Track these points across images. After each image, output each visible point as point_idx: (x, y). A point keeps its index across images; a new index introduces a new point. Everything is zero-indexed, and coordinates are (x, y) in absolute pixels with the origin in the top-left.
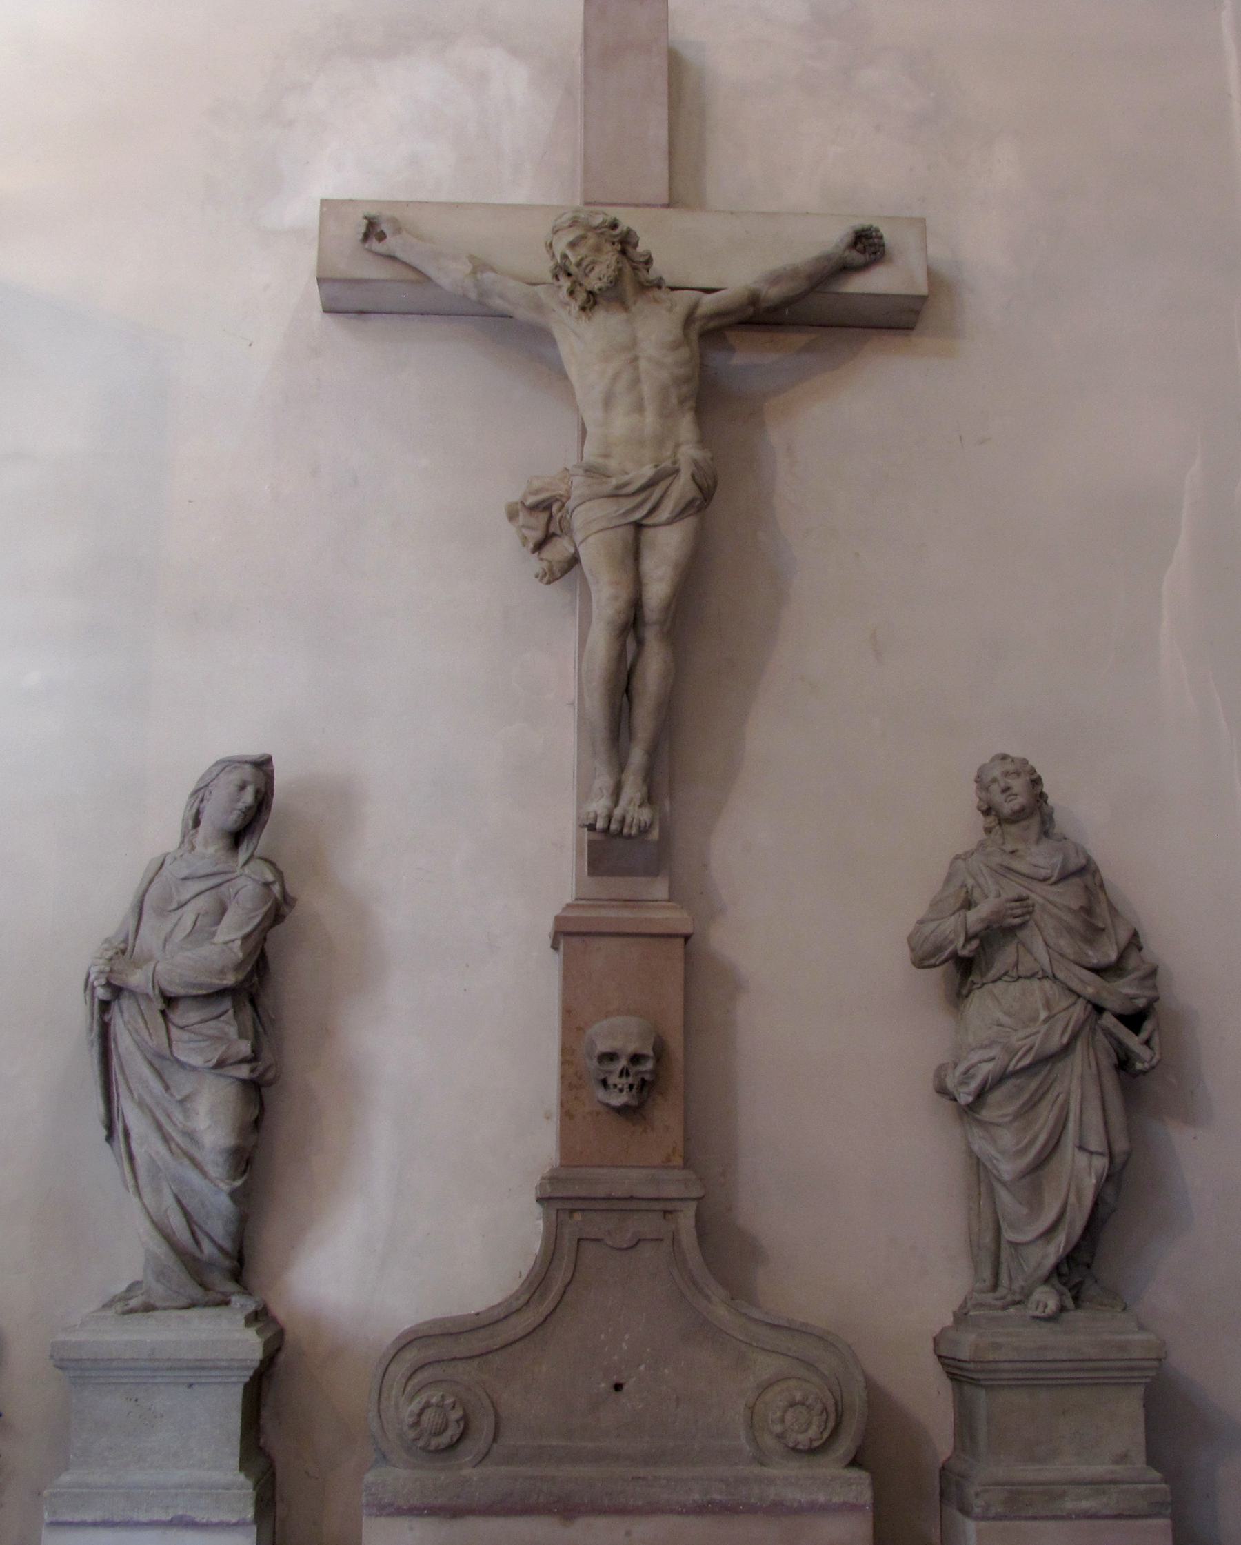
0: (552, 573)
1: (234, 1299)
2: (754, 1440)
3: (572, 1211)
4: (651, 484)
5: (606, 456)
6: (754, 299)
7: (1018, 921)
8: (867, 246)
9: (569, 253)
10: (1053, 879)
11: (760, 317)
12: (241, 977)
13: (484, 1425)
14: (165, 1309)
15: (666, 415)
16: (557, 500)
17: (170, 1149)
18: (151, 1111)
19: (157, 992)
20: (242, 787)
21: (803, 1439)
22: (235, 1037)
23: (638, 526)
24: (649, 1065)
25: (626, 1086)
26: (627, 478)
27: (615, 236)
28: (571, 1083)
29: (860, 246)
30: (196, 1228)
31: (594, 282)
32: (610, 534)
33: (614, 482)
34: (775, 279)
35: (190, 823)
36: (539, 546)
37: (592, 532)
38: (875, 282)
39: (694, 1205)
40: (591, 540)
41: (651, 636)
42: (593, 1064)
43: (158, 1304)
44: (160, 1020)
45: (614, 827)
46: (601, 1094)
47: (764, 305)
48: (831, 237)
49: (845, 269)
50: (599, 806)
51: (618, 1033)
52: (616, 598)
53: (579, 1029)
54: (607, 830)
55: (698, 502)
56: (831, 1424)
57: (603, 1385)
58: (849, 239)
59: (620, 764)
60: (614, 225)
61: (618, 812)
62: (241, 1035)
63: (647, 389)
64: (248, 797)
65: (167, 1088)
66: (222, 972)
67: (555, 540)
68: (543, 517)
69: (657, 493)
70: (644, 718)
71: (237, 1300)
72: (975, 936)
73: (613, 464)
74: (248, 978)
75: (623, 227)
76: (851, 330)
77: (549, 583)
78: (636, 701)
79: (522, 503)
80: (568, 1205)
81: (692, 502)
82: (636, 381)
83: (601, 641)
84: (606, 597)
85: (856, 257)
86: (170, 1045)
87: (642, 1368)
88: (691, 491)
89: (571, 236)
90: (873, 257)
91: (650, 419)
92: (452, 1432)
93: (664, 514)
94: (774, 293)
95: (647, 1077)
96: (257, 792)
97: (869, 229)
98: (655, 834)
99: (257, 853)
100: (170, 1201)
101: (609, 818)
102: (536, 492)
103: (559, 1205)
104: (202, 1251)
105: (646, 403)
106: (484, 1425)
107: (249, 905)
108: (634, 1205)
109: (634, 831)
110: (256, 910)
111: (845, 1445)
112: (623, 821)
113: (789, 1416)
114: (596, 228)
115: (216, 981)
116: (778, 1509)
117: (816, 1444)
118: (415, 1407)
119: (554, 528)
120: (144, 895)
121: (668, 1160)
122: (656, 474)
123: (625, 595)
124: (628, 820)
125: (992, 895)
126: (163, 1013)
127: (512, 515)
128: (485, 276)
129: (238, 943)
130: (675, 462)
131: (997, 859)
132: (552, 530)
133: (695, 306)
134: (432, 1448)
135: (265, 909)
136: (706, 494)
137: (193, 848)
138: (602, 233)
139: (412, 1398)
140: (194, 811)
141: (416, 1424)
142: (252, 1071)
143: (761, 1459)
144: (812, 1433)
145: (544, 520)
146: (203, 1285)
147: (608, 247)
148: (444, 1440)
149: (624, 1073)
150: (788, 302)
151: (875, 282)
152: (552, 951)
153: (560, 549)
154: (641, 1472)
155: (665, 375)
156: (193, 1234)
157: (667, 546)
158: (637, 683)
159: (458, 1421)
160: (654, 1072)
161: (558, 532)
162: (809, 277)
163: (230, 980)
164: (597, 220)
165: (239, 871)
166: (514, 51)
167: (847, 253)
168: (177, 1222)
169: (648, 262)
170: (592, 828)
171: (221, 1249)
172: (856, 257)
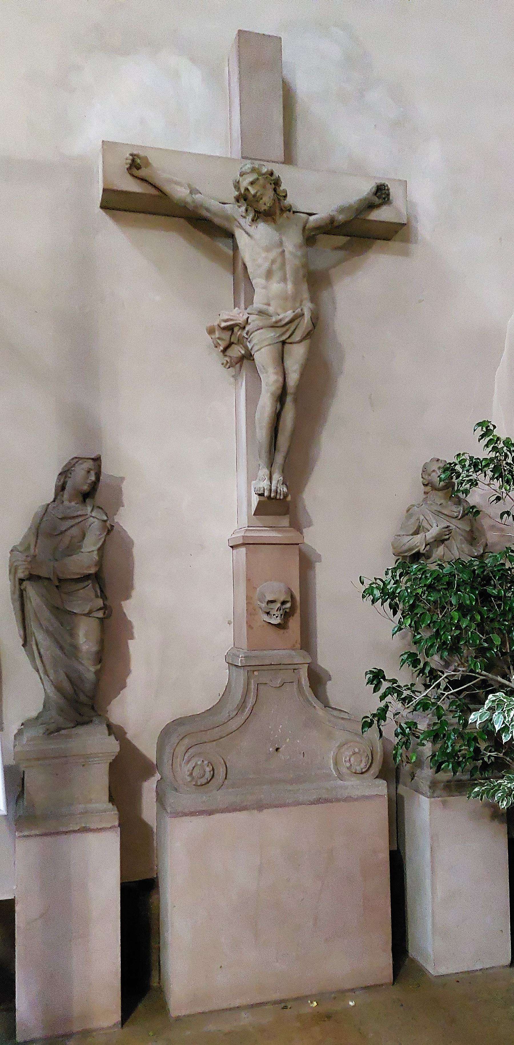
2: (337, 770)
3: (254, 671)
5: (269, 305)
6: (332, 220)
7: (447, 537)
8: (382, 194)
9: (250, 188)
10: (459, 517)
11: (331, 228)
12: (97, 569)
13: (221, 771)
21: (359, 769)
24: (288, 605)
25: (279, 615)
26: (280, 317)
28: (251, 612)
29: (379, 194)
31: (263, 208)
33: (274, 319)
34: (342, 210)
35: (60, 488)
37: (262, 346)
38: (382, 214)
39: (307, 665)
40: (263, 350)
42: (264, 605)
45: (272, 495)
46: (266, 618)
47: (336, 224)
48: (365, 188)
49: (371, 206)
50: (265, 484)
51: (274, 590)
52: (277, 381)
53: (254, 587)
54: (269, 497)
56: (370, 761)
57: (271, 749)
58: (374, 190)
59: (271, 464)
60: (272, 174)
62: (97, 596)
63: (289, 269)
66: (89, 567)
67: (233, 345)
72: (429, 544)
73: (271, 309)
75: (276, 174)
79: (218, 325)
80: (252, 668)
82: (283, 264)
84: (269, 380)
85: (377, 201)
87: (288, 740)
89: (250, 178)
92: (208, 776)
93: (297, 337)
94: (341, 218)
95: (288, 610)
97: (384, 185)
98: (289, 498)
102: (226, 321)
103: (249, 668)
106: (221, 771)
107: (98, 533)
108: (282, 667)
109: (282, 497)
110: (100, 535)
111: (375, 769)
112: (276, 492)
113: (352, 759)
116: (348, 799)
117: (364, 770)
118: (190, 766)
121: (294, 646)
123: (281, 379)
124: (279, 491)
125: (435, 525)
128: (197, 196)
129: (96, 552)
130: (302, 310)
131: (435, 508)
132: (232, 340)
133: (307, 222)
134: (199, 784)
139: (189, 761)
141: (191, 774)
143: (341, 776)
144: (363, 766)
147: (268, 186)
148: (204, 781)
149: (279, 609)
151: (382, 214)
153: (237, 351)
154: (290, 787)
157: (297, 354)
159: (210, 772)
160: (290, 608)
162: (357, 210)
163: (92, 571)
164: (264, 170)
168: (66, 685)
170: (261, 495)
172: (377, 201)
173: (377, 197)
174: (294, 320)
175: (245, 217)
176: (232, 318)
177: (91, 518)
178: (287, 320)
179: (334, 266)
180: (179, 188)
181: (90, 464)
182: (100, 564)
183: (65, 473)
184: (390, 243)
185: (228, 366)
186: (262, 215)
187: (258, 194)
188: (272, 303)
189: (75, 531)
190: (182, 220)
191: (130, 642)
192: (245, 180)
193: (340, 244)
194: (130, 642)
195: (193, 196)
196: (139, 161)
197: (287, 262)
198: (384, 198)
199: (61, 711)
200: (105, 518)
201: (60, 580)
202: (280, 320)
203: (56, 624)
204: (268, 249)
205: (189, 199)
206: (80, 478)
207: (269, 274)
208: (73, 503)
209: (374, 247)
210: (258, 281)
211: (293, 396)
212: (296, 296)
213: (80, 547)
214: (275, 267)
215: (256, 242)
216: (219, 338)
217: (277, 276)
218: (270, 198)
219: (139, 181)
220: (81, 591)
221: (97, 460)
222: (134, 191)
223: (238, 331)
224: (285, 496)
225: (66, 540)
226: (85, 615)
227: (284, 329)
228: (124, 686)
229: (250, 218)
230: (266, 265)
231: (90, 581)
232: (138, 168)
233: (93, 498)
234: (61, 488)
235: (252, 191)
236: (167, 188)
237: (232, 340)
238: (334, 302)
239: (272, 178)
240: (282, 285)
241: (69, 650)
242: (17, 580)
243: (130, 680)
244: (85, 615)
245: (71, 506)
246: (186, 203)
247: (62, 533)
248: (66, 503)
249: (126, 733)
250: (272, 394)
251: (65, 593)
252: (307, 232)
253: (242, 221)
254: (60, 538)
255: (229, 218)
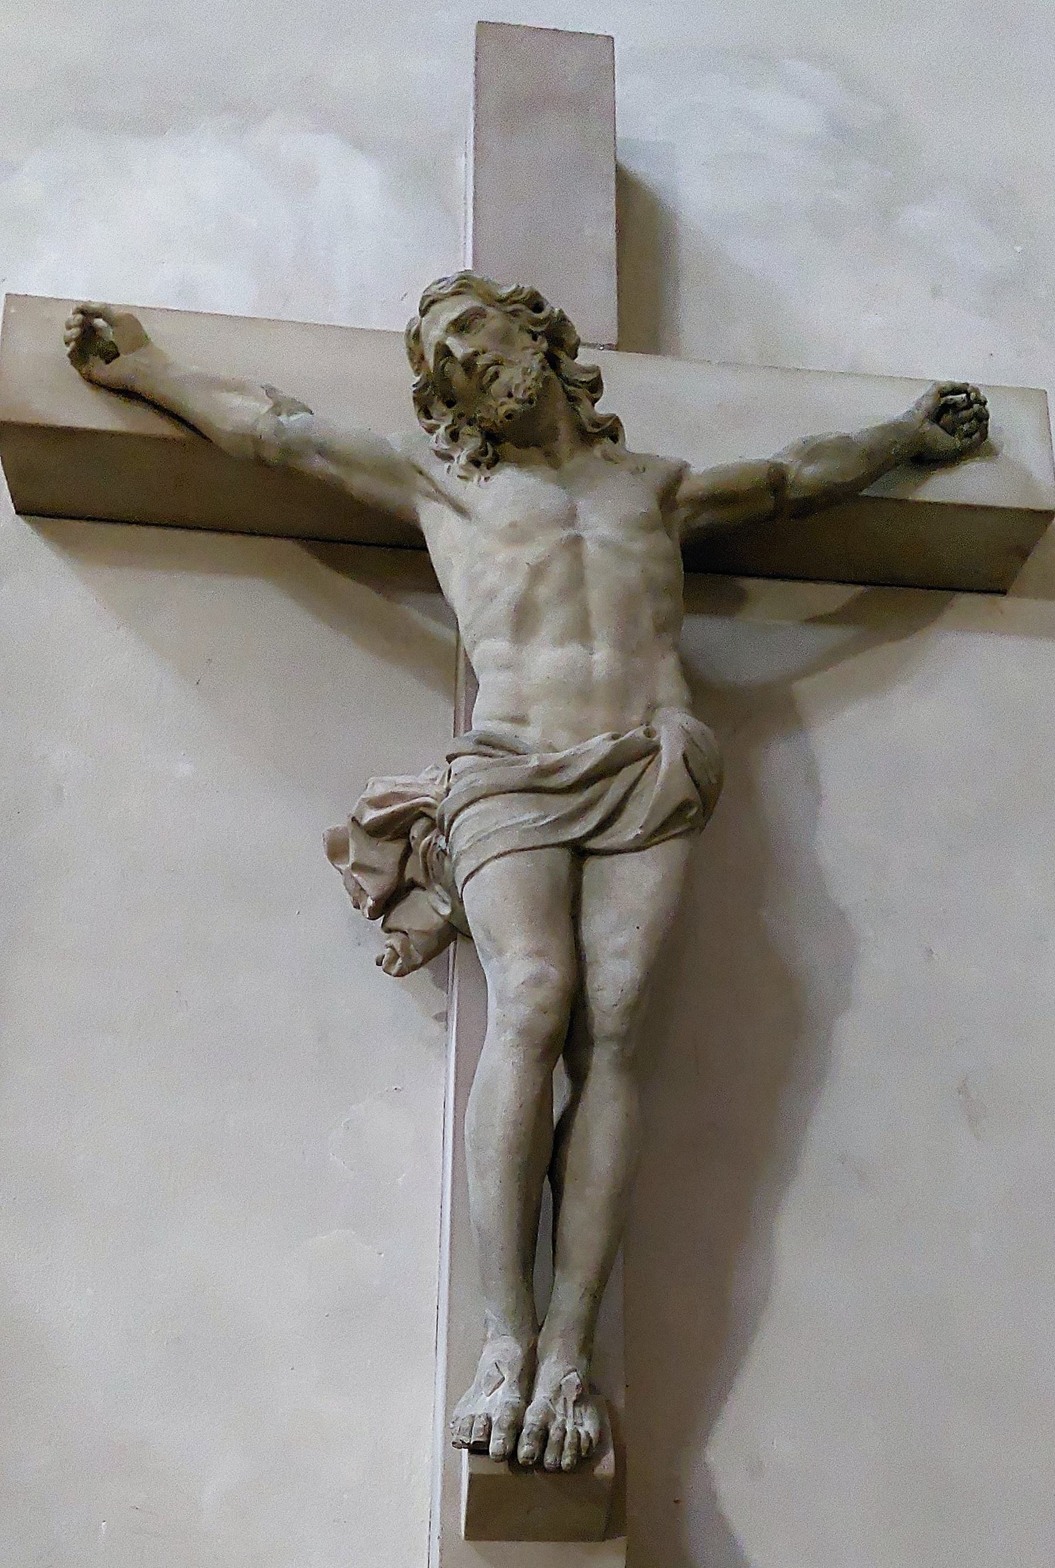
0: (408, 956)
4: (606, 770)
5: (520, 720)
8: (958, 421)
15: (627, 646)
16: (423, 815)
23: (579, 852)
27: (537, 323)
29: (947, 418)
31: (500, 406)
32: (522, 859)
33: (534, 761)
34: (812, 451)
36: (385, 906)
38: (964, 485)
41: (602, 1061)
47: (793, 495)
49: (925, 459)
50: (494, 1402)
52: (537, 981)
54: (510, 1457)
55: (692, 813)
59: (531, 1320)
61: (532, 1418)
63: (597, 597)
67: (415, 893)
68: (396, 849)
69: (616, 787)
70: (584, 1220)
73: (530, 735)
76: (912, 590)
77: (400, 974)
78: (569, 1188)
81: (683, 808)
83: (502, 1067)
84: (514, 973)
88: (682, 790)
89: (450, 311)
90: (967, 441)
91: (602, 657)
93: (628, 829)
101: (516, 1428)
102: (378, 803)
105: (595, 623)
109: (566, 1461)
114: (501, 301)
119: (414, 870)
122: (616, 749)
123: (556, 973)
124: (554, 1433)
127: (336, 851)
130: (649, 734)
132: (408, 875)
136: (702, 810)
138: (514, 313)
145: (399, 857)
150: (831, 499)
151: (964, 485)
152: (410, 408)
153: (425, 911)
155: (632, 573)
157: (629, 896)
158: (573, 1156)
161: (421, 879)
162: (870, 455)
166: (359, 144)
167: (927, 427)
169: (595, 387)
170: (478, 1449)
172: (942, 439)
173: (942, 427)
174: (619, 769)
175: (447, 457)
176: (401, 789)
178: (585, 765)
179: (807, 671)
180: (236, 400)
184: (1005, 603)
185: (394, 971)
186: (503, 441)
187: (481, 362)
188: (535, 712)
190: (288, 546)
192: (434, 321)
193: (833, 607)
195: (283, 418)
196: (110, 335)
197: (590, 576)
198: (969, 435)
202: (559, 767)
204: (517, 535)
205: (265, 428)
207: (523, 620)
209: (949, 615)
210: (487, 651)
211: (615, 1047)
212: (623, 690)
214: (544, 591)
215: (481, 531)
216: (356, 867)
217: (554, 620)
218: (525, 372)
219: (113, 399)
222: (93, 426)
223: (426, 833)
224: (587, 1456)
227: (577, 800)
229: (462, 457)
230: (512, 588)
232: (110, 355)
235: (459, 349)
236: (197, 404)
237: (408, 875)
238: (812, 780)
239: (541, 316)
240: (573, 650)
246: (257, 441)
250: (524, 1032)
252: (683, 513)
253: (439, 471)
255: (399, 471)
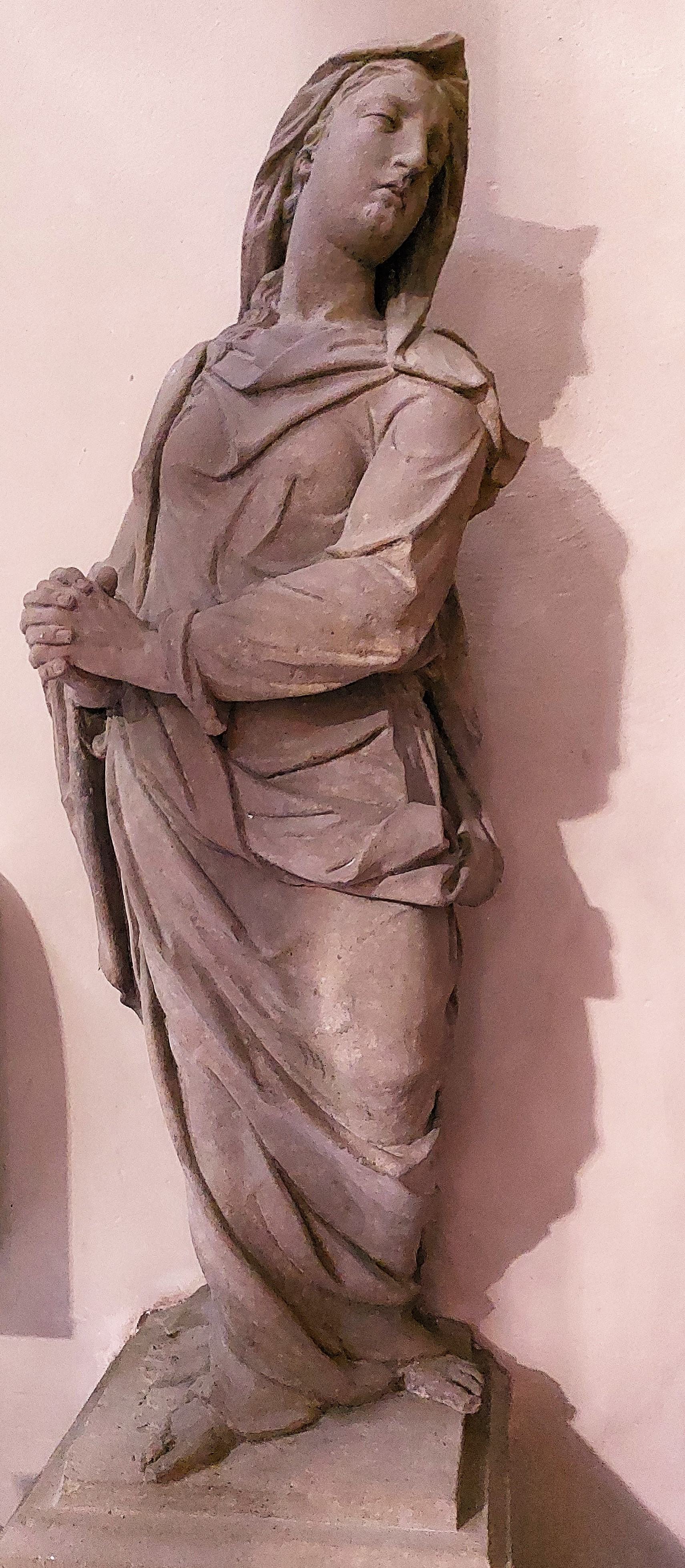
1: (412, 1373)
12: (411, 644)
14: (261, 1438)
17: (253, 1075)
18: (205, 978)
19: (198, 690)
20: (391, 123)
22: (402, 797)
30: (320, 1231)
35: (263, 253)
43: (244, 1430)
44: (212, 759)
62: (416, 792)
64: (411, 149)
65: (239, 929)
66: (364, 632)
71: (422, 1385)
74: (426, 646)
86: (240, 823)
96: (432, 140)
99: (433, 320)
100: (262, 1172)
104: (337, 1279)
110: (442, 461)
115: (349, 659)
120: (160, 447)
126: (221, 742)
129: (406, 548)
135: (464, 459)
137: (272, 318)
140: (269, 218)
142: (449, 882)
146: (342, 1356)
156: (316, 1243)
163: (387, 651)
165: (391, 358)
168: (278, 1217)
171: (382, 1270)
177: (402, 382)
181: (403, 79)
182: (445, 618)
183: (283, 166)
189: (307, 449)
191: (595, 1007)
194: (595, 1007)
199: (247, 1343)
200: (475, 379)
201: (231, 710)
203: (219, 928)
206: (356, 175)
208: (319, 317)
213: (336, 532)
220: (341, 765)
221: (442, 62)
225: (268, 491)
226: (339, 887)
228: (563, 1201)
231: (382, 717)
233: (426, 288)
234: (269, 248)
241: (272, 1062)
242: (71, 712)
243: (593, 1179)
244: (339, 887)
245: (318, 330)
247: (249, 462)
248: (288, 319)
249: (569, 1411)
251: (265, 778)
254: (236, 491)
